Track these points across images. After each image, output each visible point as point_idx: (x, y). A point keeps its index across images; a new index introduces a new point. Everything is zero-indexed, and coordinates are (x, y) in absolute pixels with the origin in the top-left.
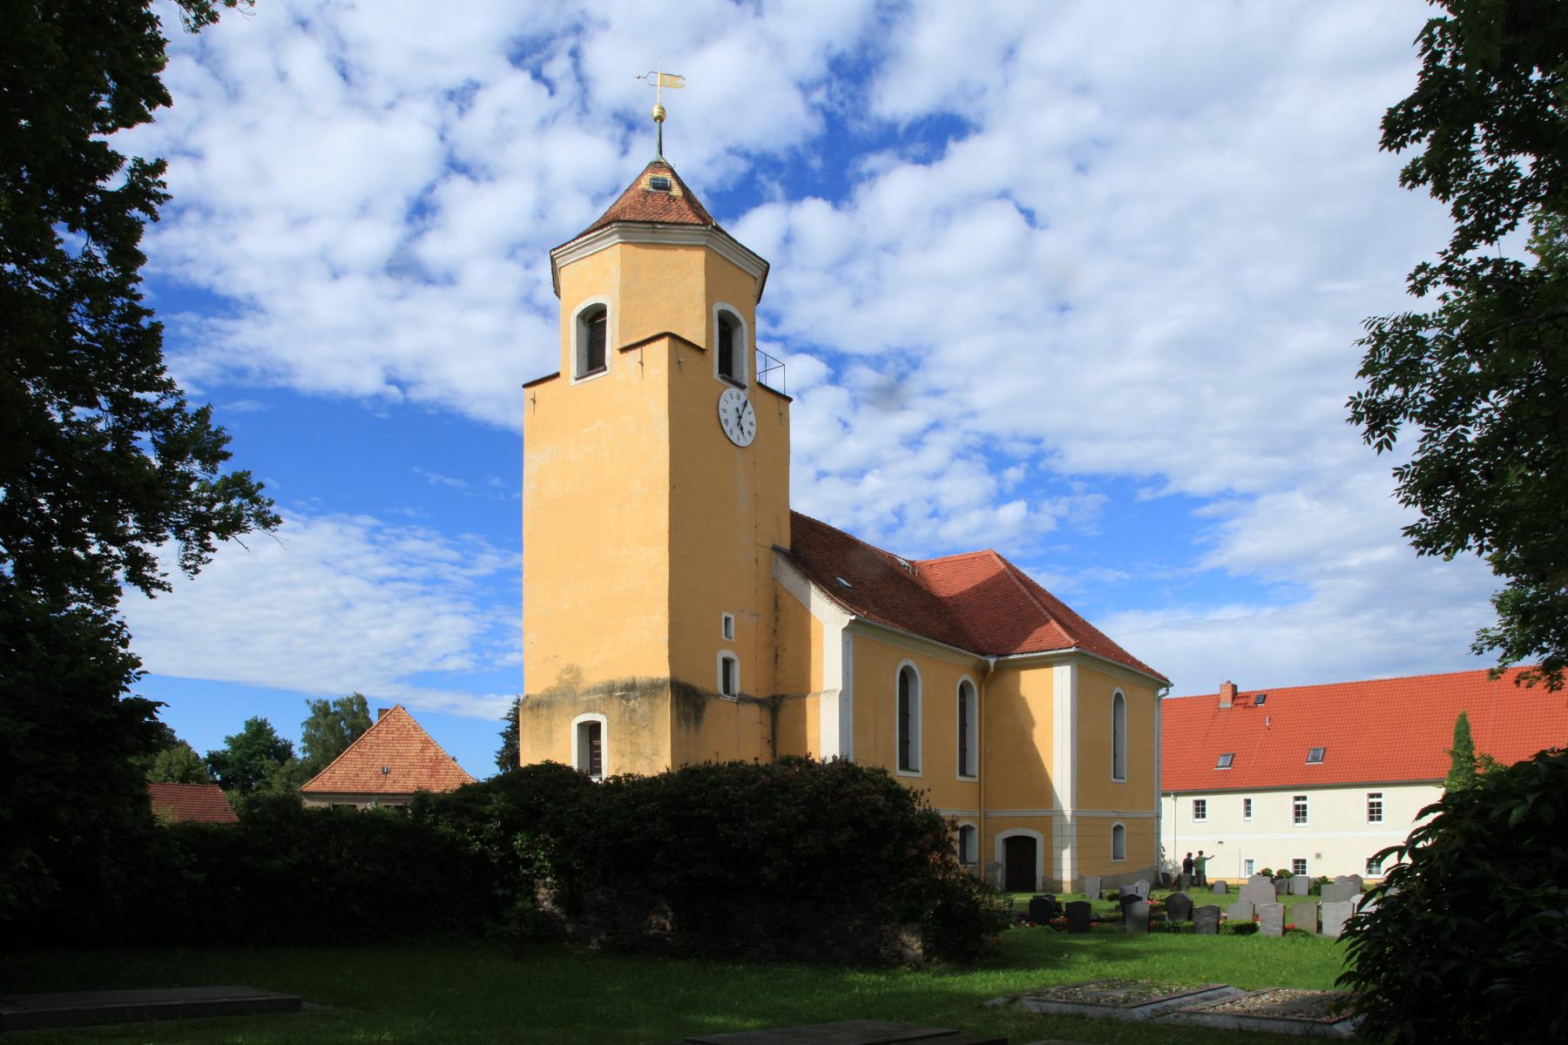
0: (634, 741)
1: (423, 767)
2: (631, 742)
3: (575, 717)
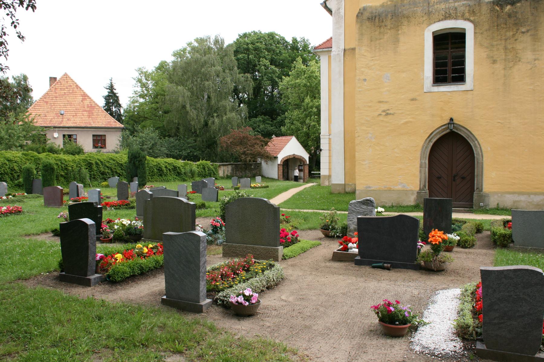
0: (509, 47)
1: (85, 111)
2: (506, 48)
3: (430, 24)
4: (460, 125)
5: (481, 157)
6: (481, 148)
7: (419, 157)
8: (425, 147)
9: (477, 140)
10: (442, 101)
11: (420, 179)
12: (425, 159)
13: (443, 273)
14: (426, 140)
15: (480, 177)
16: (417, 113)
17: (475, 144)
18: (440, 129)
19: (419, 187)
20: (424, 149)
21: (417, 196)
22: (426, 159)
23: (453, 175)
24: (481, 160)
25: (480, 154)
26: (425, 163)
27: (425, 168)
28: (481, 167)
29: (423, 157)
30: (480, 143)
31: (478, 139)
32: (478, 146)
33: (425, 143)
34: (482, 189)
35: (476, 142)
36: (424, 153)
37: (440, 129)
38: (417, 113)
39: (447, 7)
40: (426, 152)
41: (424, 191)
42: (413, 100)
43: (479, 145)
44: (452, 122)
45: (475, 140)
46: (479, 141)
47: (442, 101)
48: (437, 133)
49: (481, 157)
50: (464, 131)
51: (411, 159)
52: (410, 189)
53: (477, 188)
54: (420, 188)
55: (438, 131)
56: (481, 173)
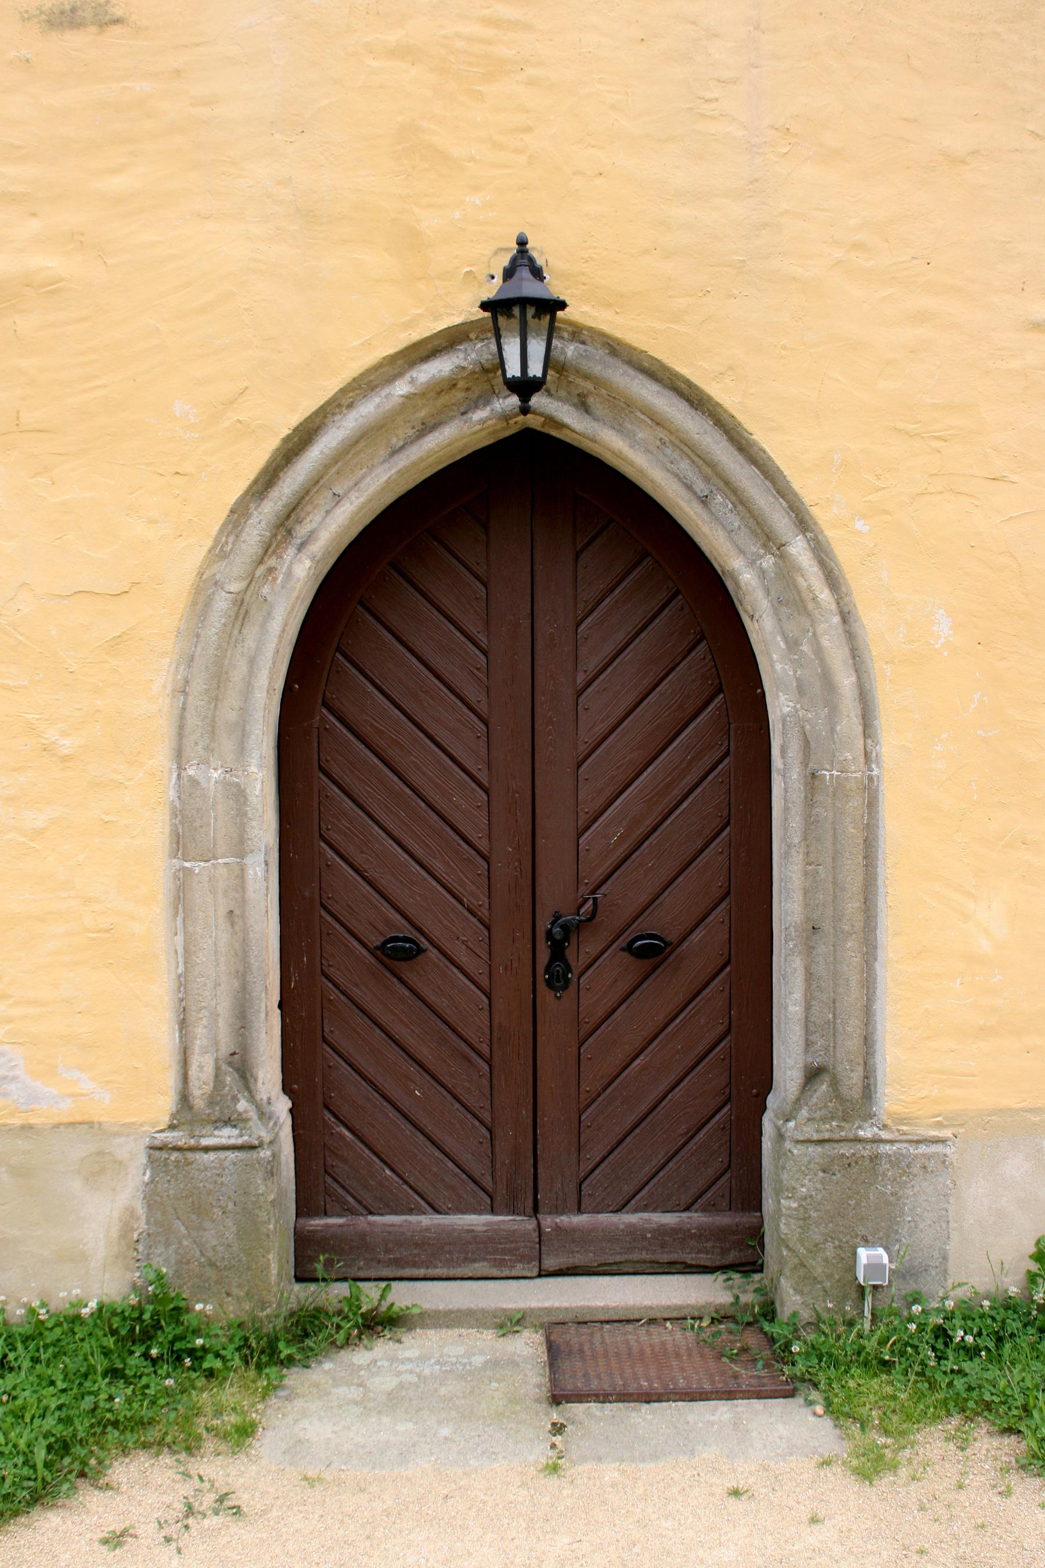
4: (615, 348)
5: (849, 722)
6: (846, 617)
7: (163, 727)
8: (222, 603)
9: (803, 522)
10: (404, 52)
11: (183, 983)
12: (227, 745)
13: (400, 1332)
14: (240, 512)
15: (852, 951)
16: (117, 183)
17: (787, 569)
18: (401, 388)
19: (170, 1080)
20: (217, 619)
21: (152, 1198)
22: (242, 750)
23: (544, 924)
24: (851, 755)
25: (846, 681)
26: (239, 795)
27: (241, 848)
28: (852, 831)
29: (212, 729)
30: (844, 555)
31: (821, 515)
32: (825, 595)
33: (219, 553)
34: (868, 1091)
35: (798, 549)
36: (219, 678)
37: (401, 388)
38: (117, 183)
39: (254, 1157)
40: (238, 674)
41: (227, 1135)
42: (736, 1493)
43: (833, 579)
44: (530, 288)
45: (781, 522)
46: (832, 534)
47: (404, 52)
48: (367, 436)
49: (849, 722)
50: (658, 421)
51: (67, 745)
52: (65, 1110)
53: (813, 1075)
54: (184, 1098)
55: (368, 410)
56: (852, 905)
